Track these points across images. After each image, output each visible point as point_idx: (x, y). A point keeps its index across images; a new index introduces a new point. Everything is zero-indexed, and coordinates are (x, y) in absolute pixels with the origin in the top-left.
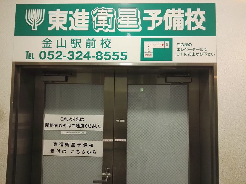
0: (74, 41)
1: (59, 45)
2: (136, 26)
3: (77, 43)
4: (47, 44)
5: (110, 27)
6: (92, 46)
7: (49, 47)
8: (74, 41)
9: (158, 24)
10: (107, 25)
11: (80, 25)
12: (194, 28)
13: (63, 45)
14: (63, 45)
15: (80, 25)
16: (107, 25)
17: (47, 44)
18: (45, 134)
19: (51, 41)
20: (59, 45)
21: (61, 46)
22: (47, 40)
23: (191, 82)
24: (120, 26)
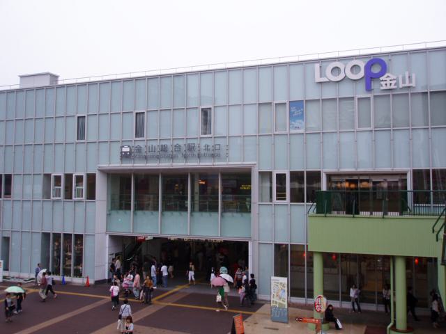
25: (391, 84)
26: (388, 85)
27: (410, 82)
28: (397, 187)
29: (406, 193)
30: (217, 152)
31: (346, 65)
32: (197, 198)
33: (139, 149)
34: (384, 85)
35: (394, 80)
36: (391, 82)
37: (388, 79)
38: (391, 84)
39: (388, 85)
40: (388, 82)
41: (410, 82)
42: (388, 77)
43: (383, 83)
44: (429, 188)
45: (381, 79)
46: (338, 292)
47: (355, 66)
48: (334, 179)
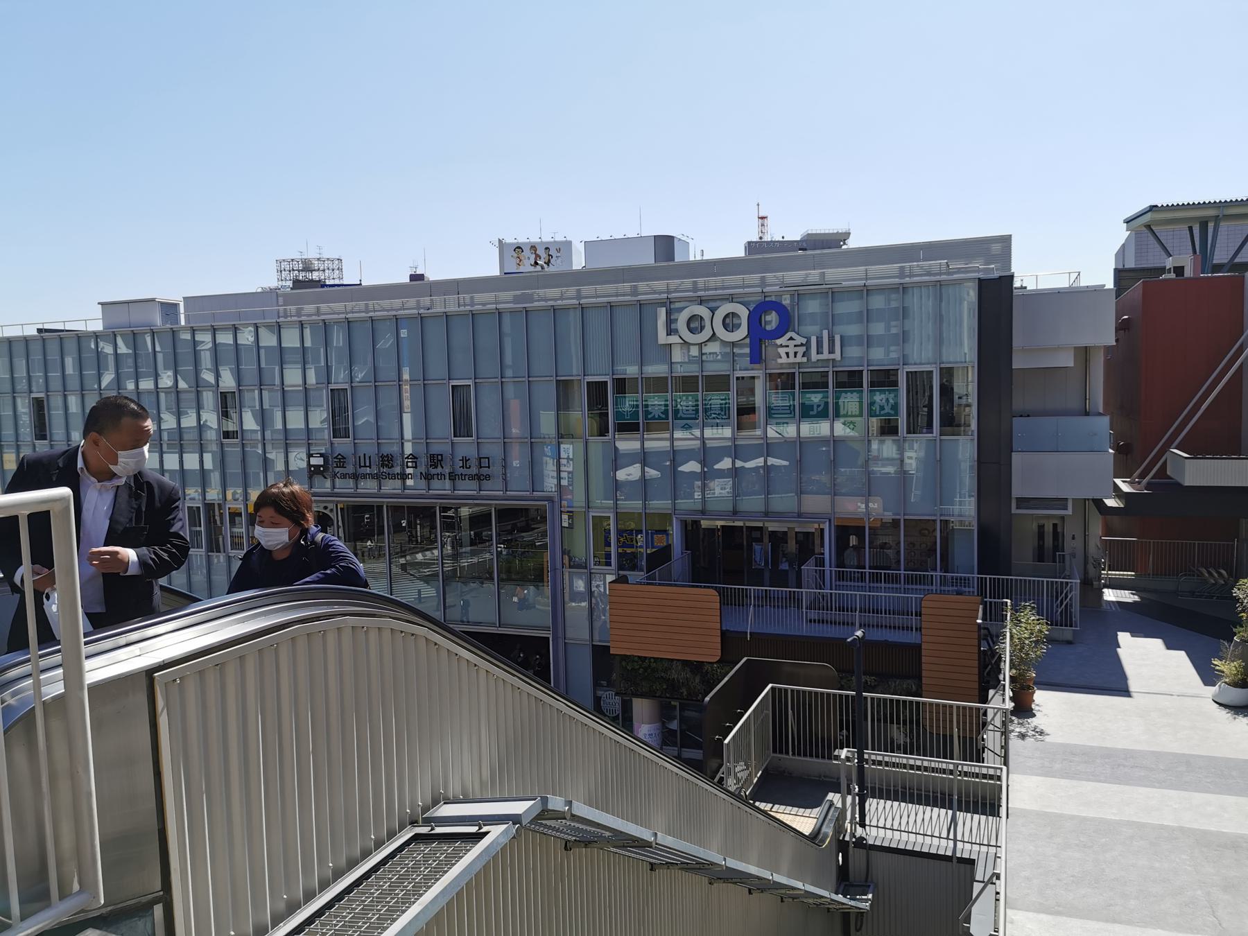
0: (433, 457)
1: (362, 464)
2: (789, 411)
3: (438, 460)
4: (340, 462)
5: (723, 413)
6: (360, 457)
7: (343, 467)
8: (433, 457)
9: (820, 409)
10: (720, 412)
11: (688, 412)
12: (882, 412)
13: (368, 464)
14: (368, 464)
15: (688, 412)
16: (720, 412)
17: (340, 462)
18: (119, 455)
19: (417, 458)
20: (362, 464)
21: (365, 466)
22: (340, 457)
23: (1069, 643)
24: (773, 412)
25: (796, 353)
26: (792, 355)
27: (831, 351)
28: (1003, 611)
29: (185, 312)
30: (484, 471)
31: (713, 311)
32: (390, 519)
33: (341, 461)
34: (784, 355)
35: (802, 345)
36: (797, 349)
37: (792, 343)
38: (796, 353)
39: (792, 355)
40: (791, 350)
41: (831, 351)
42: (791, 339)
43: (782, 351)
44: (870, 552)
45: (779, 342)
46: (929, 792)
47: (727, 316)
48: (342, 394)
